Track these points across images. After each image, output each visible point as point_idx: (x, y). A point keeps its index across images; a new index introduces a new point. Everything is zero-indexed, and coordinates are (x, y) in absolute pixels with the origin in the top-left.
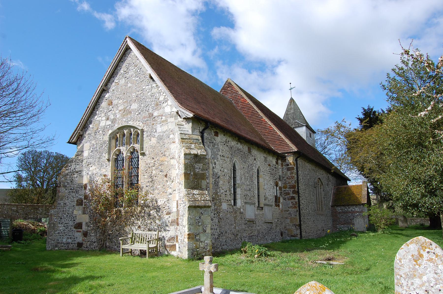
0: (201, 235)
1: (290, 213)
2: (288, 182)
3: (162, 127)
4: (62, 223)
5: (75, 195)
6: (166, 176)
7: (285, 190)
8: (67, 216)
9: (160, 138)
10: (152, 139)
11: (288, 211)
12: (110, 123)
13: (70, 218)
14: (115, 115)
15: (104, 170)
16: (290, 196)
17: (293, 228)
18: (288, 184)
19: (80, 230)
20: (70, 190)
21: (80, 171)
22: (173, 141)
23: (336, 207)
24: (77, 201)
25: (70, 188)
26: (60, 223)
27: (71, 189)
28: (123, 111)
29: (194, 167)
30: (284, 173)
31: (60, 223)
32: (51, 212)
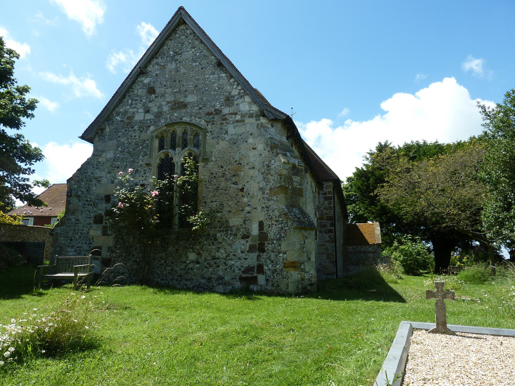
0: (306, 263)
1: (326, 248)
2: (326, 213)
3: (237, 129)
4: (72, 247)
5: (93, 208)
6: (242, 190)
7: (321, 222)
8: (80, 237)
9: (234, 142)
10: (221, 142)
11: (324, 245)
12: (152, 117)
13: (85, 239)
14: (160, 106)
15: (141, 178)
16: (327, 228)
17: (330, 265)
18: (325, 215)
19: (98, 257)
20: (85, 202)
21: (100, 177)
22: (253, 147)
23: (347, 246)
24: (95, 217)
25: (85, 199)
26: (69, 246)
27: (87, 201)
28: (173, 103)
29: (293, 180)
30: (321, 203)
31: (69, 246)
32: (57, 230)
